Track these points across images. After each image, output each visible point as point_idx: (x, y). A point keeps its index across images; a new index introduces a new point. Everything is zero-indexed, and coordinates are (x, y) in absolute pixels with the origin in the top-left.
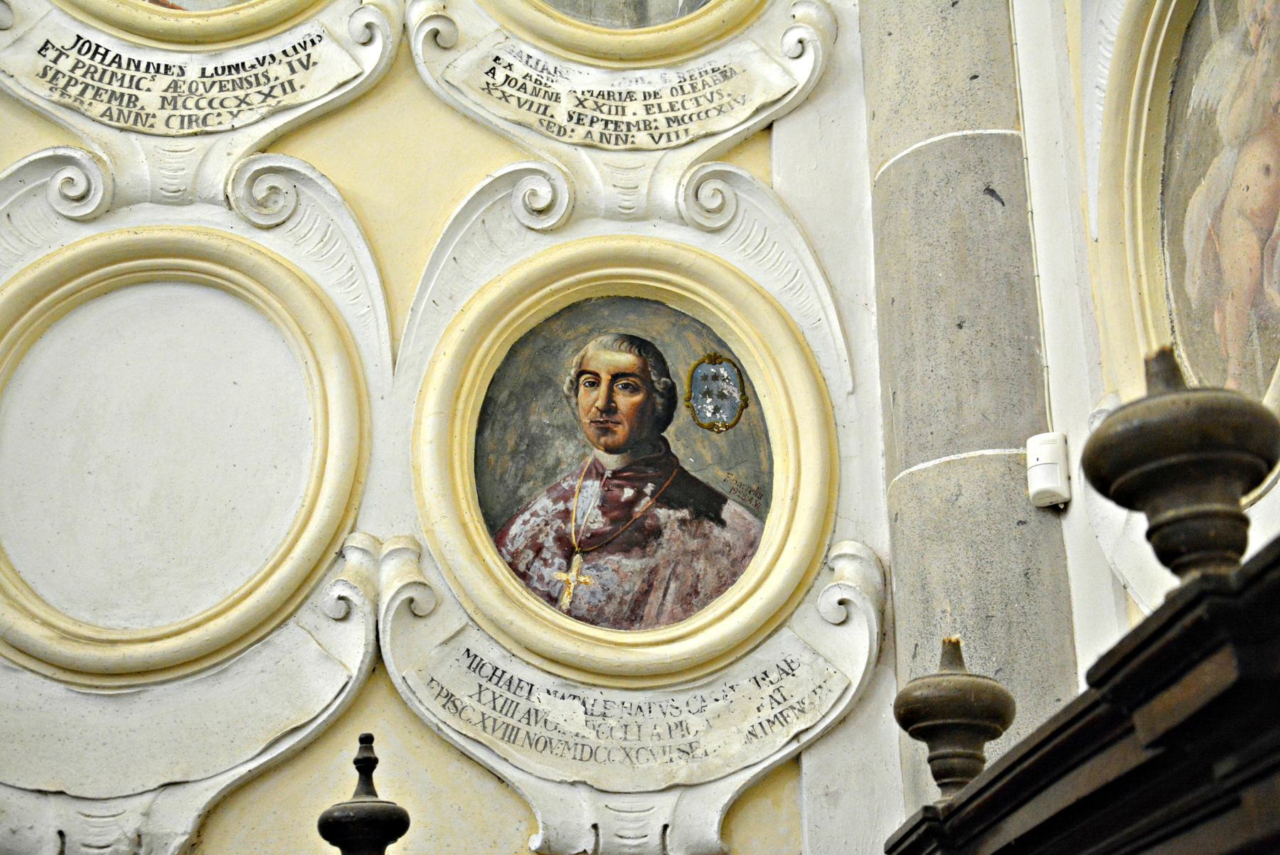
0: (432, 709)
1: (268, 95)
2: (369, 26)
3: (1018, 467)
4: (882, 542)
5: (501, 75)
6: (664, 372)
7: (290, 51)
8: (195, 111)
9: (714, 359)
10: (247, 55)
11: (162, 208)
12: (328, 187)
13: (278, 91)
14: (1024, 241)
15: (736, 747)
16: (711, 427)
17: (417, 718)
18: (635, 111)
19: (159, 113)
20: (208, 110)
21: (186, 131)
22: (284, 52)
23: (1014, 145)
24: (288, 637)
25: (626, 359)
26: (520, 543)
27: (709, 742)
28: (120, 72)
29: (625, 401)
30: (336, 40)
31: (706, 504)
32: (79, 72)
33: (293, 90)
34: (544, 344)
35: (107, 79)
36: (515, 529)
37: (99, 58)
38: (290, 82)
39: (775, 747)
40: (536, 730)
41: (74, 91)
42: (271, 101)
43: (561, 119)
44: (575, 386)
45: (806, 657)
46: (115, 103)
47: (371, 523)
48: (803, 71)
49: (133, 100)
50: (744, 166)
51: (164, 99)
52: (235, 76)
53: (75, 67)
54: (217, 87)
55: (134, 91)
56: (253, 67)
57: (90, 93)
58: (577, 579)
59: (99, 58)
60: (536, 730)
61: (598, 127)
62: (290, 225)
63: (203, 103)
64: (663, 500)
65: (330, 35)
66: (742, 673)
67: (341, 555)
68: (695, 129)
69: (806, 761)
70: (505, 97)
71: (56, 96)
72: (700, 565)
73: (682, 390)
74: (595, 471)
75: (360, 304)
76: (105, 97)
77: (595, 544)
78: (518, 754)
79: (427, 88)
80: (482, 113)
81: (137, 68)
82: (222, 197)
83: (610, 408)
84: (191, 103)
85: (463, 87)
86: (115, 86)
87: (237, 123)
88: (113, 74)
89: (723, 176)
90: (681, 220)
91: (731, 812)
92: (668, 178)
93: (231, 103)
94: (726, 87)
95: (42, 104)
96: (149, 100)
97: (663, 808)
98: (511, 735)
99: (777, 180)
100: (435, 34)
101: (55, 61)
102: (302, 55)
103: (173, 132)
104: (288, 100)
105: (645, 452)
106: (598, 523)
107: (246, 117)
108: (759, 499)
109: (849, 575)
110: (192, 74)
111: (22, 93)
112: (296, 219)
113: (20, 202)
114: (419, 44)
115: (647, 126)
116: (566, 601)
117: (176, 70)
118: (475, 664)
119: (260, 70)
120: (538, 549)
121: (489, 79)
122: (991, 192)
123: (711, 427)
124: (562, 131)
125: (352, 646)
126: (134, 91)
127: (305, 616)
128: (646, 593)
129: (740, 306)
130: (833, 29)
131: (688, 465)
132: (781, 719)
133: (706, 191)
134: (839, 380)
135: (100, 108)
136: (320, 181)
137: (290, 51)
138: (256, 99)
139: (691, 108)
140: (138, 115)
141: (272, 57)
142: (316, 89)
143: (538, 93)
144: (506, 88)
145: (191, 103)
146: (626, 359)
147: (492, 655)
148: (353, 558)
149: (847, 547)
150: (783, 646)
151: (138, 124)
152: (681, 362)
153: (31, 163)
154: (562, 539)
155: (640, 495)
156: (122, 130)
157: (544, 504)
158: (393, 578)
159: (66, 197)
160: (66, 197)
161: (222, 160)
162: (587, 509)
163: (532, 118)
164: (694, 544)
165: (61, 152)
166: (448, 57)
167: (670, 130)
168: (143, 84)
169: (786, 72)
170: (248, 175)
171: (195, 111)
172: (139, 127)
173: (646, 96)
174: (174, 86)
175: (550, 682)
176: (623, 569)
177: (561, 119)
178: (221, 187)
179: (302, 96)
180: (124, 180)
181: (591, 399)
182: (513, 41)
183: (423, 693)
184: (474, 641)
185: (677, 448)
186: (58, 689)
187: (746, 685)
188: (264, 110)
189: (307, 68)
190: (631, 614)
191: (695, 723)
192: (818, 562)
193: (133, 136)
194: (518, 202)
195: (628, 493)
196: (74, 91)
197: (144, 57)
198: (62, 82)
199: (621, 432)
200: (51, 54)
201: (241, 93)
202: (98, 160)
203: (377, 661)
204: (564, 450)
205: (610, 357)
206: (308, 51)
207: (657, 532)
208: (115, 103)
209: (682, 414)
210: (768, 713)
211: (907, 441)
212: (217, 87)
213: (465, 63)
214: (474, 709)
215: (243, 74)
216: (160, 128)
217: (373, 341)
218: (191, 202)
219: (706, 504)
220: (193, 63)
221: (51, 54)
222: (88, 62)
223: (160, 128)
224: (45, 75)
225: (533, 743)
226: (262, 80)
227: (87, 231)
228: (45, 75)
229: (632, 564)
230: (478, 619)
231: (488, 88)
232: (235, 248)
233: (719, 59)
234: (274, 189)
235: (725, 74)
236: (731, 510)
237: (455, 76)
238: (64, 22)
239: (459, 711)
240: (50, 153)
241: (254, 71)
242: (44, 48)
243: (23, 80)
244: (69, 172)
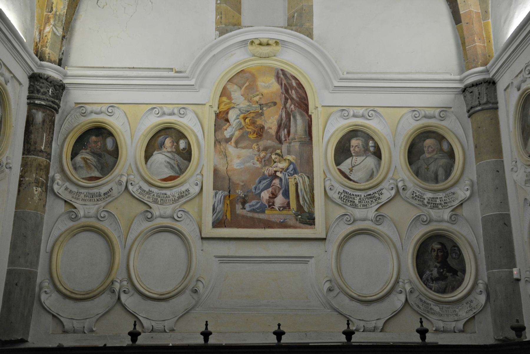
0: (416, 308)
3: (512, 273)
4: (486, 279)
6: (446, 249)
9: (454, 246)
10: (371, 192)
14: (511, 232)
15: (464, 314)
16: (455, 258)
17: (414, 310)
18: (438, 201)
23: (508, 215)
24: (392, 296)
25: (439, 246)
26: (425, 279)
27: (460, 313)
29: (440, 254)
30: (386, 189)
31: (454, 272)
34: (358, 198)
36: (424, 277)
39: (471, 314)
40: (432, 311)
41: (345, 201)
43: (426, 203)
44: (431, 251)
45: (475, 300)
47: (402, 277)
48: (468, 193)
49: (354, 202)
50: (458, 212)
58: (434, 285)
60: (432, 311)
61: (432, 205)
64: (447, 272)
66: (464, 302)
67: (398, 282)
68: (449, 205)
69: (476, 317)
70: (416, 199)
72: (455, 283)
73: (449, 252)
74: (436, 267)
75: (395, 238)
77: (437, 279)
78: (431, 316)
79: (402, 198)
83: (437, 255)
89: (455, 214)
90: (448, 222)
91: (464, 325)
92: (446, 214)
94: (454, 196)
96: (357, 202)
97: (454, 324)
98: (428, 312)
99: (464, 214)
105: (444, 263)
106: (437, 275)
107: (373, 205)
108: (464, 271)
109: (481, 286)
110: (363, 196)
113: (339, 222)
114: (401, 191)
115: (441, 204)
116: (433, 289)
118: (421, 300)
120: (428, 280)
122: (505, 224)
123: (455, 258)
124: (426, 206)
125: (402, 298)
127: (394, 293)
128: (446, 287)
130: (472, 185)
131: (451, 265)
132: (471, 310)
133: (453, 217)
134: (477, 251)
135: (349, 204)
138: (374, 201)
139: (448, 201)
142: (384, 198)
143: (420, 198)
146: (439, 246)
147: (424, 299)
148: (401, 283)
149: (480, 281)
150: (470, 298)
151: (355, 206)
152: (449, 247)
154: (431, 278)
155: (444, 271)
157: (428, 272)
158: (408, 287)
161: (371, 213)
162: (435, 272)
163: (421, 203)
164: (453, 279)
166: (406, 191)
167: (445, 205)
169: (465, 194)
173: (440, 198)
174: (360, 199)
175: (433, 303)
176: (442, 284)
177: (426, 203)
180: (355, 217)
181: (434, 254)
183: (414, 305)
184: (421, 297)
185: (449, 262)
186: (359, 304)
187: (465, 304)
190: (444, 291)
191: (457, 310)
192: (475, 284)
194: (420, 219)
195: (442, 270)
196: (345, 201)
197: (355, 194)
199: (440, 259)
203: (406, 300)
204: (431, 263)
205: (436, 246)
207: (447, 277)
209: (450, 257)
210: (469, 309)
211: (490, 265)
213: (408, 194)
214: (422, 308)
217: (399, 245)
219: (454, 272)
220: (363, 194)
223: (359, 207)
225: (432, 313)
229: (443, 283)
230: (421, 293)
231: (413, 198)
233: (452, 190)
235: (454, 194)
236: (459, 273)
237: (407, 196)
238: (341, 188)
239: (420, 308)
244: (347, 216)
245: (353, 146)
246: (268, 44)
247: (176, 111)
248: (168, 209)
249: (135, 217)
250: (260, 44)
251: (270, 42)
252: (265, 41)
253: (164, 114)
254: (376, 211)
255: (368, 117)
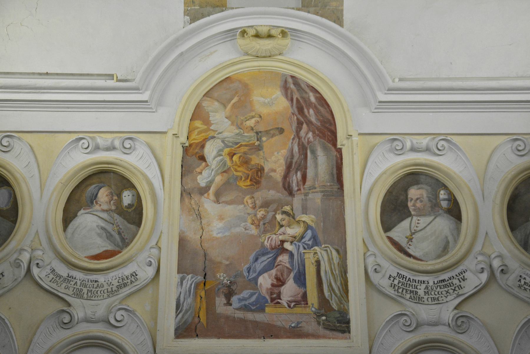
1: (454, 290)
2: (482, 268)
5: (523, 282)
7: (458, 275)
8: (434, 296)
10: (445, 276)
11: (430, 327)
12: (478, 321)
13: (457, 289)
19: (424, 297)
20: (438, 296)
21: (434, 303)
22: (456, 275)
28: (411, 284)
30: (471, 271)
32: (400, 284)
33: (462, 288)
35: (408, 286)
37: (404, 279)
38: (460, 285)
41: (400, 290)
42: (456, 292)
46: (412, 294)
49: (416, 293)
51: (425, 292)
52: (443, 284)
53: (399, 283)
54: (439, 288)
55: (416, 290)
56: (448, 280)
57: (404, 291)
59: (404, 279)
62: (468, 332)
63: (436, 293)
65: (470, 270)
70: (525, 289)
71: (396, 293)
76: (409, 292)
80: (520, 295)
81: (415, 282)
82: (447, 324)
84: (433, 293)
85: (513, 287)
86: (411, 288)
87: (448, 299)
88: (409, 284)
93: (444, 293)
95: (391, 295)
96: (421, 292)
100: (502, 270)
101: (393, 281)
102: (462, 276)
103: (430, 303)
104: (461, 292)
107: (450, 298)
110: (431, 283)
111: (388, 293)
112: (469, 331)
114: (498, 274)
117: (426, 282)
119: (450, 281)
121: (519, 283)
126: (416, 290)
129: (134, 173)
135: (408, 296)
136: (476, 319)
137: (458, 275)
138: (451, 291)
140: (419, 298)
141: (453, 277)
142: (469, 287)
144: (525, 286)
145: (433, 293)
151: (419, 300)
153: (395, 316)
156: (415, 303)
159: (404, 325)
160: (404, 325)
161: (447, 312)
165: (403, 312)
168: (418, 287)
170: (455, 318)
171: (434, 296)
172: (420, 302)
174: (427, 288)
178: (447, 321)
179: (465, 290)
182: (525, 270)
188: (455, 295)
189: (464, 280)
193: (419, 305)
197: (417, 279)
198: (396, 288)
200: (392, 279)
201: (446, 289)
202: (413, 315)
206: (464, 274)
208: (412, 294)
212: (439, 288)
215: (446, 283)
216: (426, 302)
218: (438, 325)
220: (431, 280)
221: (392, 279)
222: (402, 281)
223: (426, 302)
224: (392, 286)
226: (452, 285)
227: (411, 335)
228: (392, 286)
231: (520, 286)
232: (455, 341)
234: (462, 322)
237: (510, 283)
240: (400, 312)
241: (448, 282)
242: (390, 277)
243: (387, 288)
244: (405, 318)
245: (412, 199)
246: (270, 36)
247: (117, 143)
248: (100, 307)
249: (42, 321)
250: (257, 36)
251: (273, 32)
252: (264, 31)
253: (97, 148)
254: (456, 308)
255: (438, 152)
